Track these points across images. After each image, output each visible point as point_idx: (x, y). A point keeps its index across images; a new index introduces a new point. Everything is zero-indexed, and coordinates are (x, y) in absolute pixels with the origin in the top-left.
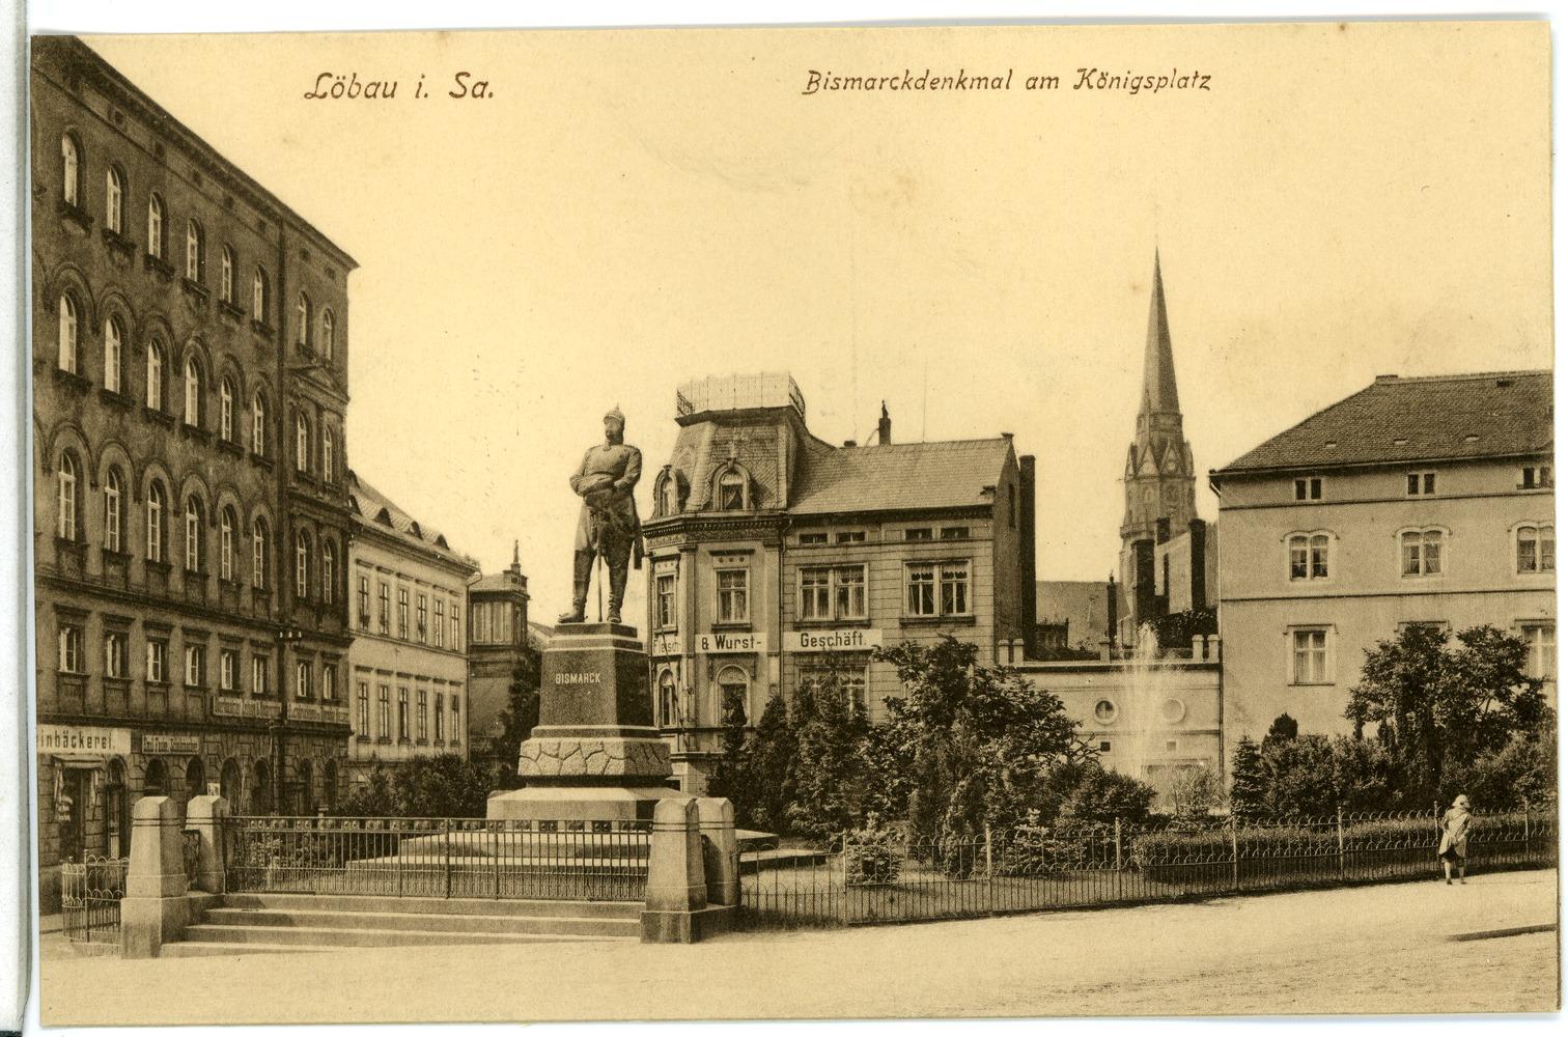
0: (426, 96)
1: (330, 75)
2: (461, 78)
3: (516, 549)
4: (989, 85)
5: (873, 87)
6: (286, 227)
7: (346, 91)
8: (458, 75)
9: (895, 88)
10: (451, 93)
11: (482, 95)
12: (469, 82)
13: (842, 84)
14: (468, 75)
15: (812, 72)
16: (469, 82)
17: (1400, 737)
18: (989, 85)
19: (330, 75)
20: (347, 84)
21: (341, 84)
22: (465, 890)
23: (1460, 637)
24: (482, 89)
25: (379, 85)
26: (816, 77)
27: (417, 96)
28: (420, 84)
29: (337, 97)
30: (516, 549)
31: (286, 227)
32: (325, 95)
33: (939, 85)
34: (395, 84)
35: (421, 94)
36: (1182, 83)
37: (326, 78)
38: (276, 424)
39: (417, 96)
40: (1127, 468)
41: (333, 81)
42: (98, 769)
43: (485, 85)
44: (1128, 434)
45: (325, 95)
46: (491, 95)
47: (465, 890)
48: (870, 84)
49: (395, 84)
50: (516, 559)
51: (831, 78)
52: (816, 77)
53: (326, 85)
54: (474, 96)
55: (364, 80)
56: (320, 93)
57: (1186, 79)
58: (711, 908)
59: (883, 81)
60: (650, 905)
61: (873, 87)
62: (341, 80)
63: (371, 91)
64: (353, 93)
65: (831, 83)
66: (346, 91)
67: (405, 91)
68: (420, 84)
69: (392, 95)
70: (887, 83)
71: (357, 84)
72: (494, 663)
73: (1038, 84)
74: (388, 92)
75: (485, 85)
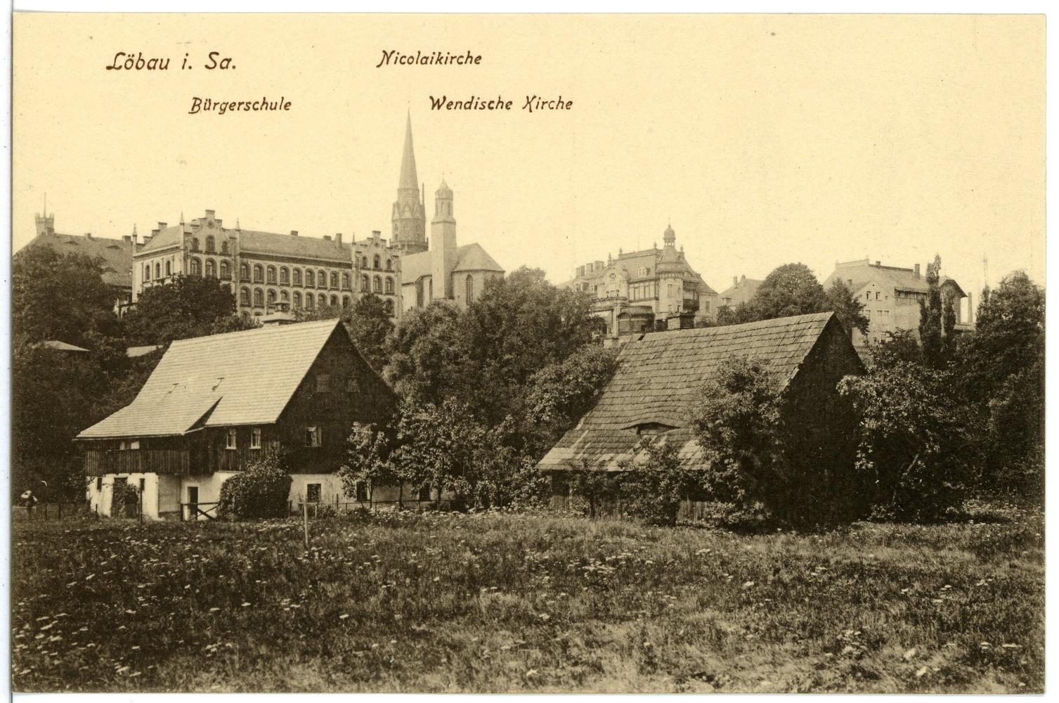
1: (123, 54)
2: (213, 56)
4: (564, 107)
5: (154, 68)
7: (135, 64)
9: (461, 63)
10: (378, 66)
11: (227, 67)
12: (218, 59)
14: (217, 54)
15: (196, 99)
18: (564, 107)
19: (123, 54)
27: (183, 68)
28: (185, 60)
32: (120, 67)
33: (453, 107)
34: (168, 60)
36: (424, 61)
37: (121, 56)
39: (183, 68)
41: (126, 58)
43: (229, 60)
45: (120, 67)
46: (234, 67)
49: (168, 60)
51: (399, 57)
52: (198, 102)
53: (121, 61)
54: (222, 68)
55: (147, 58)
56: (117, 66)
57: (427, 58)
59: (215, 104)
61: (426, 63)
63: (152, 64)
65: (479, 105)
66: (135, 64)
67: (175, 66)
68: (185, 60)
69: (166, 67)
70: (546, 105)
71: (143, 60)
73: (429, 61)
75: (229, 60)
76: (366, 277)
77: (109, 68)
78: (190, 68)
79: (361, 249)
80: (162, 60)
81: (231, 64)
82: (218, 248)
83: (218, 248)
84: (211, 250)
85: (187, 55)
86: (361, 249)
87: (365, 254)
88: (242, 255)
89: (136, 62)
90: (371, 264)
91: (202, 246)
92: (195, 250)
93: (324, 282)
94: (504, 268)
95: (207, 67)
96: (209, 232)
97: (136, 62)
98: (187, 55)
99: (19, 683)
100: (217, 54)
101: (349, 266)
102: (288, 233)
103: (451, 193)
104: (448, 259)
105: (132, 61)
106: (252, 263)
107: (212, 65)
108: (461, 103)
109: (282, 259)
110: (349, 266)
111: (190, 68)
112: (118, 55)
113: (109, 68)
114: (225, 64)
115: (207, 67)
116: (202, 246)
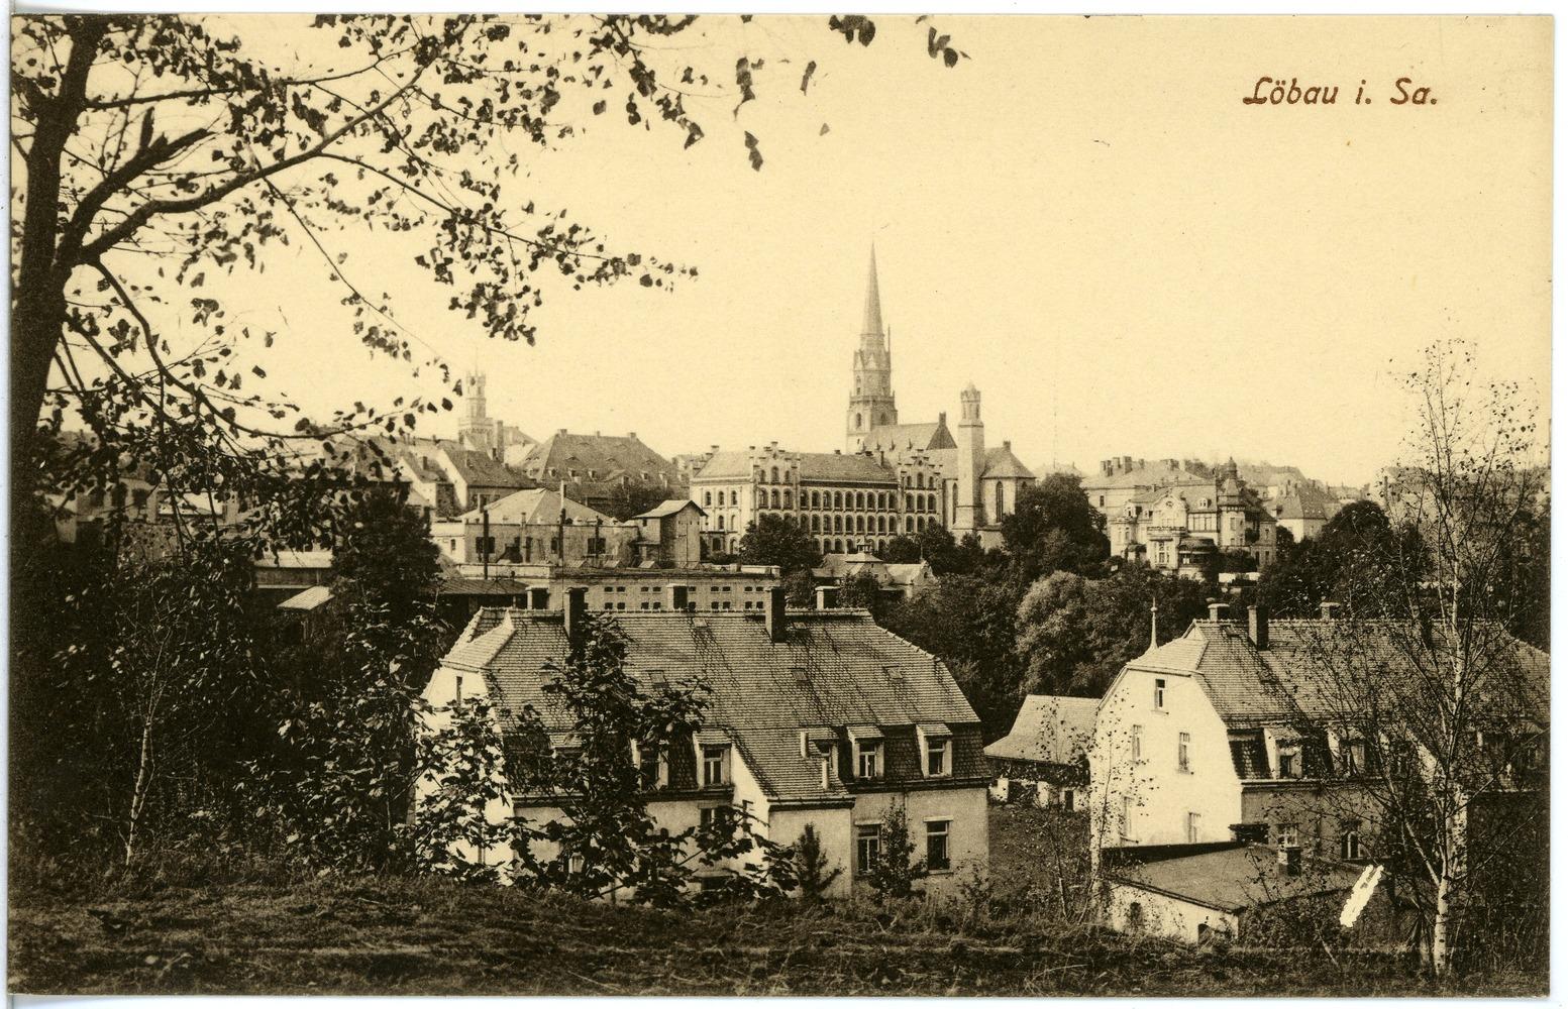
1: (1269, 80)
3: (873, 261)
5: (1314, 101)
6: (640, 37)
8: (1398, 82)
14: (1407, 80)
16: (1410, 89)
19: (1269, 80)
20: (1287, 88)
21: (1281, 89)
23: (809, 829)
24: (1422, 96)
27: (1358, 101)
28: (1361, 90)
30: (873, 261)
31: (640, 37)
34: (1336, 90)
35: (1363, 100)
39: (1358, 101)
40: (856, 362)
41: (1273, 85)
43: (1425, 91)
44: (856, 344)
49: (1336, 90)
55: (1304, 86)
58: (567, 624)
61: (1314, 101)
63: (1311, 96)
67: (1346, 97)
68: (1361, 90)
69: (1332, 100)
72: (279, 945)
74: (1328, 97)
76: (765, 493)
77: (1247, 101)
78: (1368, 101)
79: (906, 468)
80: (1326, 89)
82: (782, 479)
83: (782, 479)
84: (788, 483)
85: (1364, 82)
86: (759, 463)
87: (763, 467)
88: (803, 483)
89: (1290, 93)
90: (914, 484)
91: (769, 478)
92: (763, 482)
93: (829, 504)
94: (1035, 474)
95: (1393, 100)
96: (772, 463)
97: (1290, 93)
98: (1364, 82)
99: (38, 968)
100: (1407, 80)
101: (895, 487)
102: (831, 451)
103: (977, 393)
104: (976, 466)
105: (1281, 89)
106: (810, 490)
107: (1401, 97)
108: (1325, 101)
109: (856, 485)
110: (895, 487)
111: (1368, 101)
112: (1263, 79)
113: (1247, 101)
114: (1420, 96)
115: (1393, 100)
116: (769, 478)
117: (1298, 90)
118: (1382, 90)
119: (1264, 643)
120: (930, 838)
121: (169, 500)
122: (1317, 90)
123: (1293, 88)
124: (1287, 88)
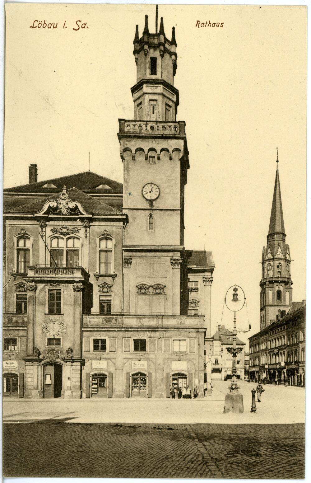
0: (88, 27)
1: (37, 21)
2: (78, 23)
11: (84, 27)
13: (220, 25)
14: (80, 21)
15: (198, 21)
17: (31, 206)
19: (37, 21)
20: (43, 23)
22: (93, 391)
25: (52, 24)
26: (199, 23)
27: (64, 28)
28: (64, 24)
29: (40, 27)
32: (36, 27)
34: (57, 24)
35: (65, 27)
37: (36, 22)
38: (285, 255)
39: (64, 28)
41: (39, 23)
42: (67, 305)
43: (85, 24)
45: (36, 27)
47: (93, 391)
48: (213, 25)
49: (57, 24)
50: (235, 317)
53: (36, 24)
54: (82, 28)
55: (212, 22)
56: (34, 26)
57: (204, 24)
60: (69, 353)
61: (214, 26)
62: (41, 22)
64: (44, 26)
67: (60, 26)
68: (64, 24)
69: (56, 27)
74: (55, 26)
75: (85, 24)
81: (86, 26)
89: (43, 25)
95: (74, 29)
97: (43, 25)
98: (65, 22)
100: (80, 21)
108: (217, 26)
112: (35, 21)
115: (74, 29)
117: (211, 24)
118: (72, 25)
119: (288, 279)
120: (122, 193)
121: (146, 47)
122: (215, 24)
123: (209, 23)
124: (43, 23)
